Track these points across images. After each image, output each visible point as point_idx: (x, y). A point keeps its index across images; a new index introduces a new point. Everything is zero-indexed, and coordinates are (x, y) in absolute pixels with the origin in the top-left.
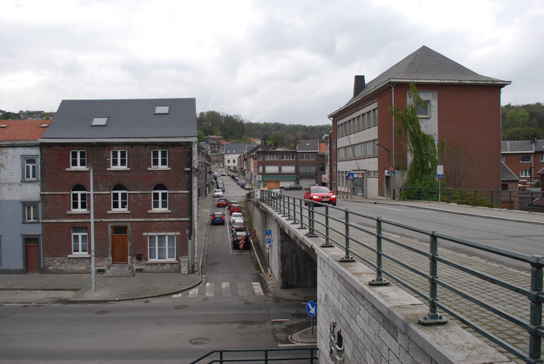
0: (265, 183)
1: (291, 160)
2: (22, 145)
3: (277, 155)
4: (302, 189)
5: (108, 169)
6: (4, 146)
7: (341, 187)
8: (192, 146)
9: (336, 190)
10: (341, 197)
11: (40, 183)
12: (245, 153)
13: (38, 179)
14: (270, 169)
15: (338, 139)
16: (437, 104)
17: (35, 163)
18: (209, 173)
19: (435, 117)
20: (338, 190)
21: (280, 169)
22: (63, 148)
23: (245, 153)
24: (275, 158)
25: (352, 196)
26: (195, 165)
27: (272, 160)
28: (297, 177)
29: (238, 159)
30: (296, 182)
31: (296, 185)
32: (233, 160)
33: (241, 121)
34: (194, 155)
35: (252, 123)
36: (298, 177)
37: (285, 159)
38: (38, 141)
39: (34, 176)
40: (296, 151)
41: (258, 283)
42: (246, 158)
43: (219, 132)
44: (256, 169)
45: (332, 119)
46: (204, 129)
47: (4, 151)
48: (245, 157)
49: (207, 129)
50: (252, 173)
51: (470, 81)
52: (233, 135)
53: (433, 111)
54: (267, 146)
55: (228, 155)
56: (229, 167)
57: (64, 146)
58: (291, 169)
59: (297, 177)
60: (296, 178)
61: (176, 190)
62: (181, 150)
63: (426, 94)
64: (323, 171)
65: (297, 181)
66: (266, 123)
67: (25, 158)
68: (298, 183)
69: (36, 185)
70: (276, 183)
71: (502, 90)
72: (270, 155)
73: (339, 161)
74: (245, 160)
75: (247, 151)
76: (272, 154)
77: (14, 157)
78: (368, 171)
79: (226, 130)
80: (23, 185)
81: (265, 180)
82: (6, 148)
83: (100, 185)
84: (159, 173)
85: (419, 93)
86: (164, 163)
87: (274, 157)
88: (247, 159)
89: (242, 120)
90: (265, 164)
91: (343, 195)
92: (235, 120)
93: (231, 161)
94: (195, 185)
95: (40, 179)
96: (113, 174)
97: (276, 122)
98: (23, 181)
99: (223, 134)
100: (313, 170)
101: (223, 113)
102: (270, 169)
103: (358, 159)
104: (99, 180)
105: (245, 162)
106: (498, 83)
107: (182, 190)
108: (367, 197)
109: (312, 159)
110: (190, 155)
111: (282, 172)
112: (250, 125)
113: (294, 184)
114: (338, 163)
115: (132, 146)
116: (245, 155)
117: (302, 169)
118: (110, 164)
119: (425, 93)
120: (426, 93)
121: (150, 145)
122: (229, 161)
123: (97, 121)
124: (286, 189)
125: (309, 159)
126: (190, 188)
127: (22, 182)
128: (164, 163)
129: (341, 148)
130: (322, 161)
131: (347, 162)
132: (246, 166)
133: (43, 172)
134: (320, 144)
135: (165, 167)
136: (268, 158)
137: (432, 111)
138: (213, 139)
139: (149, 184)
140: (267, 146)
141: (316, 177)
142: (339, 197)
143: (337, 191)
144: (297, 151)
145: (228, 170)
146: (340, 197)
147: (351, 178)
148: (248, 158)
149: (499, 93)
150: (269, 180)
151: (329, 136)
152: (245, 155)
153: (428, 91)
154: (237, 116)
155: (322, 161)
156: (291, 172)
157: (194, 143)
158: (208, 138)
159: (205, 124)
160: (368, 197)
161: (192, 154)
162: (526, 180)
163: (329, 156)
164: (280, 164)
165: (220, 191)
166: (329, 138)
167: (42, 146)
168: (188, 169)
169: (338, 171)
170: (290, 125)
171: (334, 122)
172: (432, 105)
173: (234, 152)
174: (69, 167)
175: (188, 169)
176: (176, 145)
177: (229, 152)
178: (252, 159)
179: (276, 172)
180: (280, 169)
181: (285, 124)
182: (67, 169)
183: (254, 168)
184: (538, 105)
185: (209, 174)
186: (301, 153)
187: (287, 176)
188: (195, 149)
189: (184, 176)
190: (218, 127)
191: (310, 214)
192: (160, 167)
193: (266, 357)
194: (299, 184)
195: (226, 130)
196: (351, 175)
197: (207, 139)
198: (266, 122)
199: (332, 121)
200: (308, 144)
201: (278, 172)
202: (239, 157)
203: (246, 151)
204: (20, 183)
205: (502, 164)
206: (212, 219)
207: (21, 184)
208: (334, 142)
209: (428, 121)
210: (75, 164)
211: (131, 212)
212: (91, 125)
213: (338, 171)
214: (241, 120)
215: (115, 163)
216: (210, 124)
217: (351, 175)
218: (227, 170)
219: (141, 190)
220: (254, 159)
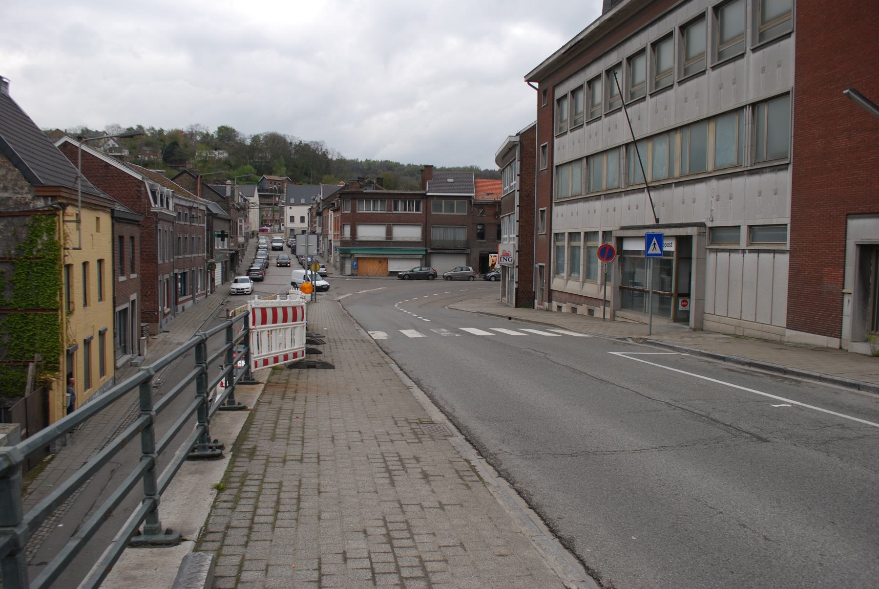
0: (355, 264)
1: (415, 212)
3: (383, 201)
4: (437, 277)
7: (584, 282)
9: (545, 288)
10: (564, 310)
12: (319, 201)
14: (369, 232)
15: (556, 141)
18: (219, 236)
20: (552, 288)
21: (389, 232)
23: (319, 201)
24: (379, 209)
25: (618, 313)
27: (372, 211)
28: (426, 251)
29: (308, 214)
30: (424, 262)
31: (423, 269)
32: (301, 217)
33: (324, 152)
35: (345, 160)
36: (429, 251)
37: (400, 210)
40: (425, 195)
42: (321, 210)
43: (284, 169)
44: (339, 233)
45: (536, 85)
46: (257, 164)
48: (319, 208)
49: (264, 164)
50: (331, 240)
52: (310, 177)
54: (362, 183)
55: (291, 208)
56: (292, 230)
58: (413, 233)
59: (426, 251)
60: (424, 253)
64: (483, 239)
65: (426, 260)
66: (370, 161)
68: (428, 265)
70: (380, 262)
71: (207, 343)
72: (368, 201)
73: (559, 204)
74: (319, 214)
75: (323, 196)
76: (372, 198)
78: (711, 228)
79: (297, 167)
81: (356, 256)
87: (376, 206)
88: (323, 212)
89: (327, 150)
90: (356, 220)
91: (574, 305)
92: (314, 151)
93: (297, 219)
97: (385, 160)
99: (291, 174)
100: (461, 235)
101: (292, 136)
102: (369, 232)
103: (655, 188)
105: (318, 217)
108: (702, 323)
109: (460, 211)
111: (394, 240)
112: (342, 162)
113: (419, 265)
114: (556, 210)
116: (318, 204)
117: (438, 234)
122: (292, 219)
124: (402, 277)
125: (454, 212)
129: (570, 163)
130: (482, 216)
131: (597, 205)
132: (319, 226)
134: (476, 180)
136: (363, 208)
138: (271, 181)
140: (362, 183)
141: (468, 251)
142: (555, 309)
143: (550, 292)
144: (428, 194)
145: (290, 235)
146: (559, 308)
147: (655, 252)
148: (323, 209)
150: (364, 256)
151: (520, 142)
152: (318, 204)
154: (317, 143)
155: (482, 216)
156: (412, 240)
158: (262, 179)
159: (260, 155)
160: (709, 324)
163: (517, 194)
164: (389, 222)
165: (247, 279)
166: (518, 148)
169: (554, 231)
170: (409, 165)
171: (545, 92)
173: (303, 201)
177: (292, 201)
178: (331, 212)
179: (380, 239)
180: (389, 232)
181: (401, 163)
183: (335, 230)
185: (220, 239)
186: (435, 198)
187: (405, 249)
190: (282, 160)
194: (430, 267)
195: (297, 167)
196: (654, 239)
197: (260, 182)
198: (368, 159)
199: (536, 92)
200: (452, 180)
201: (384, 239)
202: (310, 210)
203: (321, 196)
208: (544, 152)
213: (556, 234)
214: (324, 150)
216: (269, 156)
217: (654, 239)
218: (288, 236)
220: (334, 211)
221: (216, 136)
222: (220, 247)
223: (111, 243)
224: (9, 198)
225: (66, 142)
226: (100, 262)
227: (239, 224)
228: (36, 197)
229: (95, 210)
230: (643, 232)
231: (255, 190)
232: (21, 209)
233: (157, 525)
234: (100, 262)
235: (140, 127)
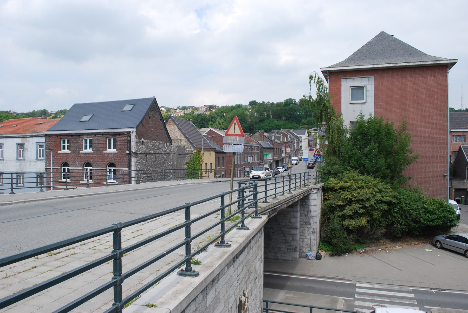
2: (37, 136)
5: (81, 152)
6: (28, 136)
8: (131, 135)
11: (45, 161)
13: (44, 158)
16: (373, 89)
17: (43, 148)
19: (372, 102)
22: (57, 138)
34: (132, 141)
38: (43, 133)
39: (43, 157)
47: (28, 140)
51: (407, 63)
53: (369, 96)
57: (57, 136)
61: (121, 167)
62: (124, 138)
63: (361, 79)
67: (38, 144)
69: (43, 162)
77: (32, 143)
80: (37, 162)
82: (29, 138)
83: (77, 163)
84: (111, 155)
85: (355, 79)
94: (133, 164)
95: (45, 158)
96: (84, 155)
98: (37, 159)
104: (76, 159)
106: (441, 62)
107: (125, 167)
110: (129, 141)
115: (95, 135)
118: (83, 148)
119: (360, 78)
120: (362, 78)
121: (105, 134)
123: (86, 118)
126: (129, 166)
127: (36, 160)
133: (46, 154)
135: (115, 151)
137: (367, 96)
139: (104, 162)
147: (319, 161)
149: (447, 72)
153: (364, 77)
157: (132, 132)
161: (131, 141)
167: (46, 136)
168: (128, 152)
172: (368, 89)
174: (106, 150)
175: (128, 152)
176: (121, 134)
182: (59, 152)
184: (302, 101)
189: (126, 157)
191: (240, 194)
196: (319, 158)
204: (35, 161)
207: (36, 161)
209: (363, 106)
211: (94, 182)
212: (80, 121)
215: (86, 148)
219: (100, 167)
221: (298, 104)
222: (265, 159)
223: (215, 159)
224: (190, 150)
225: (211, 129)
226: (211, 163)
227: (282, 149)
228: (194, 150)
229: (209, 151)
230: (26, 185)
231: (305, 132)
232: (192, 152)
233: (244, 225)
234: (211, 163)
235: (264, 102)
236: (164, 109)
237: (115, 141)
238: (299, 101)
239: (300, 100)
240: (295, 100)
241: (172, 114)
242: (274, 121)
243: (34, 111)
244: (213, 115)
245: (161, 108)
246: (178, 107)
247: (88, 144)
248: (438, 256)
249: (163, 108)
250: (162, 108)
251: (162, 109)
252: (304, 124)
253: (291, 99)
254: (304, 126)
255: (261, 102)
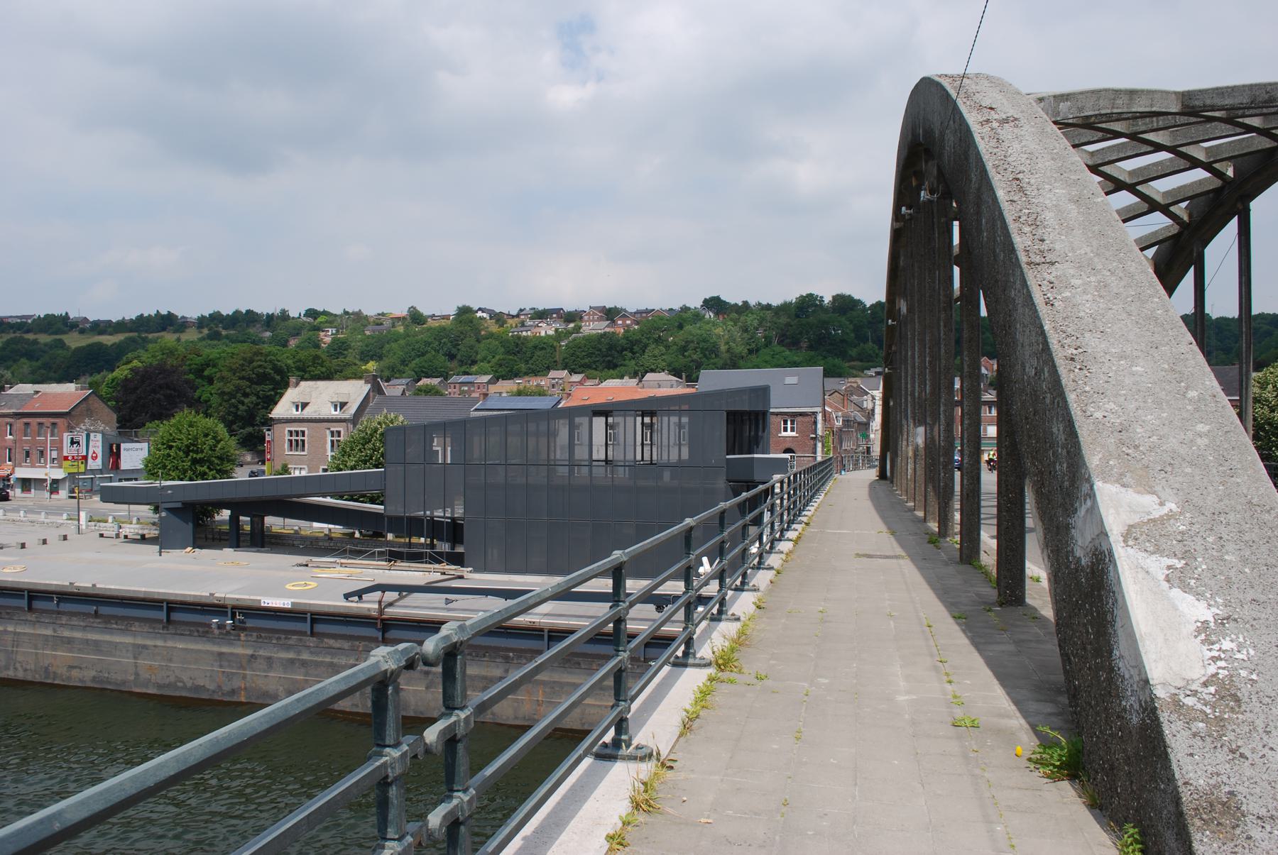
26: (820, 432)
41: (429, 817)
62: (807, 419)
86: (792, 430)
110: (815, 423)
128: (792, 430)
135: (794, 434)
162: (952, 225)
175: (814, 436)
188: (820, 417)
192: (789, 433)
193: (591, 472)
205: (1192, 250)
206: (1084, 803)
210: (785, 430)
236: (485, 315)
237: (792, 423)
238: (831, 299)
239: (833, 297)
240: (822, 297)
241: (522, 332)
242: (784, 352)
243: (142, 315)
244: (635, 337)
245: (477, 312)
246: (521, 310)
247: (789, 425)
248: (984, 312)
249: (483, 312)
250: (480, 312)
251: (479, 314)
252: (853, 359)
253: (811, 295)
254: (853, 363)
255: (740, 304)
